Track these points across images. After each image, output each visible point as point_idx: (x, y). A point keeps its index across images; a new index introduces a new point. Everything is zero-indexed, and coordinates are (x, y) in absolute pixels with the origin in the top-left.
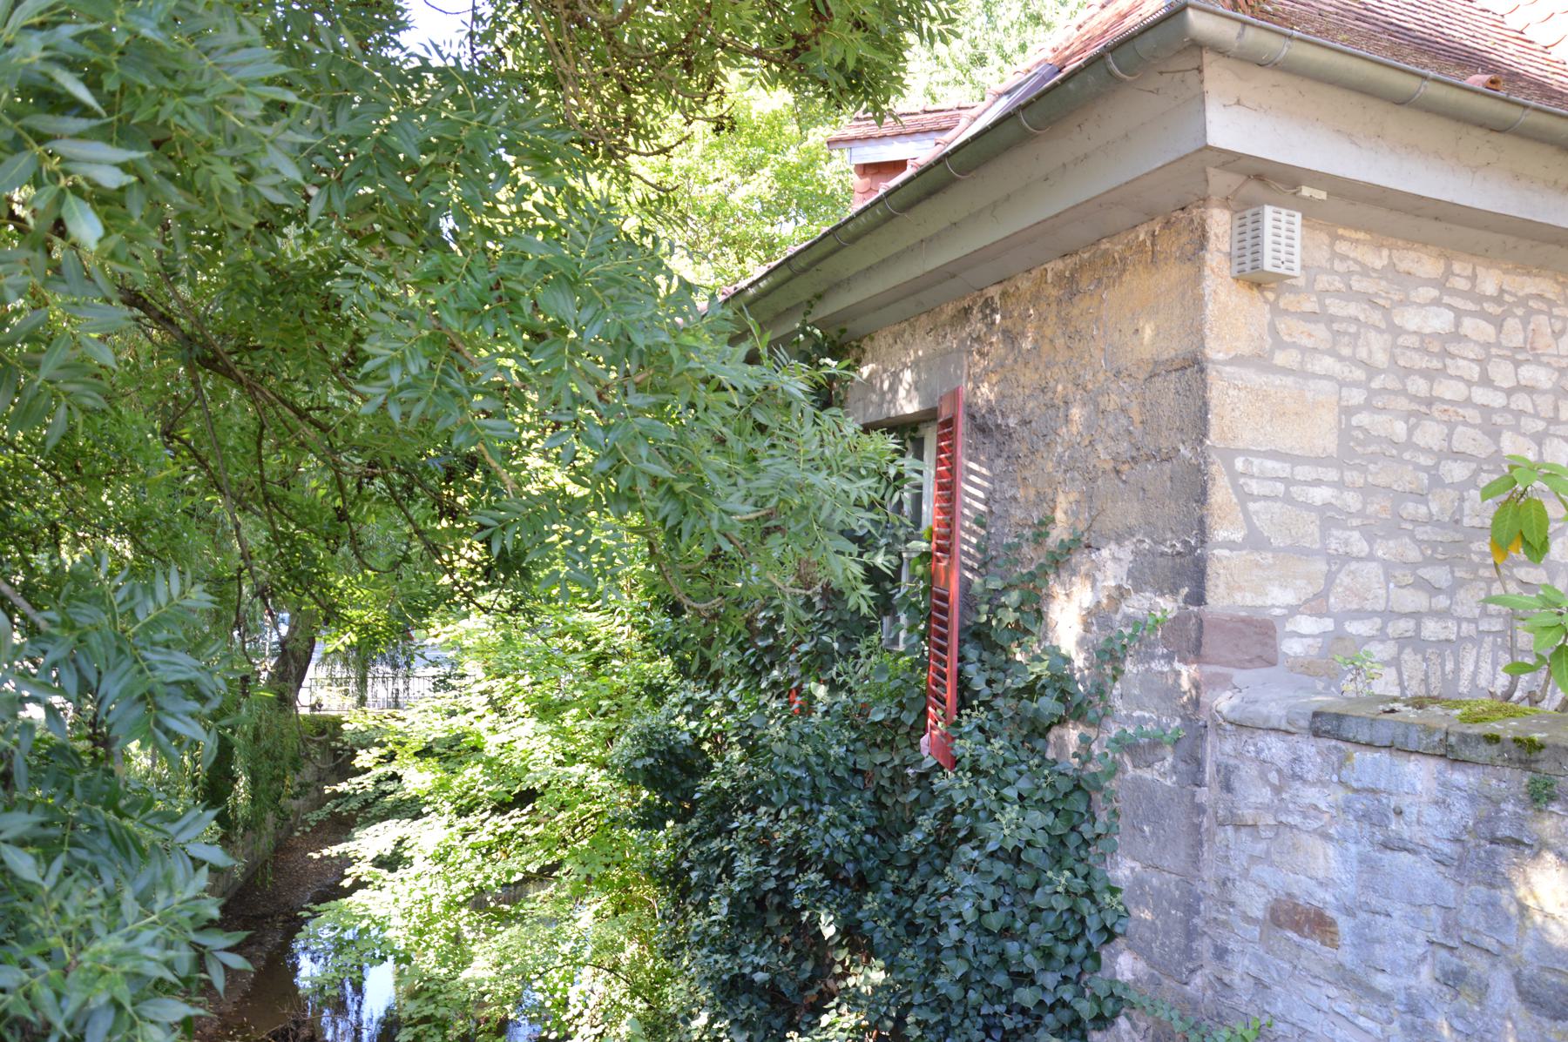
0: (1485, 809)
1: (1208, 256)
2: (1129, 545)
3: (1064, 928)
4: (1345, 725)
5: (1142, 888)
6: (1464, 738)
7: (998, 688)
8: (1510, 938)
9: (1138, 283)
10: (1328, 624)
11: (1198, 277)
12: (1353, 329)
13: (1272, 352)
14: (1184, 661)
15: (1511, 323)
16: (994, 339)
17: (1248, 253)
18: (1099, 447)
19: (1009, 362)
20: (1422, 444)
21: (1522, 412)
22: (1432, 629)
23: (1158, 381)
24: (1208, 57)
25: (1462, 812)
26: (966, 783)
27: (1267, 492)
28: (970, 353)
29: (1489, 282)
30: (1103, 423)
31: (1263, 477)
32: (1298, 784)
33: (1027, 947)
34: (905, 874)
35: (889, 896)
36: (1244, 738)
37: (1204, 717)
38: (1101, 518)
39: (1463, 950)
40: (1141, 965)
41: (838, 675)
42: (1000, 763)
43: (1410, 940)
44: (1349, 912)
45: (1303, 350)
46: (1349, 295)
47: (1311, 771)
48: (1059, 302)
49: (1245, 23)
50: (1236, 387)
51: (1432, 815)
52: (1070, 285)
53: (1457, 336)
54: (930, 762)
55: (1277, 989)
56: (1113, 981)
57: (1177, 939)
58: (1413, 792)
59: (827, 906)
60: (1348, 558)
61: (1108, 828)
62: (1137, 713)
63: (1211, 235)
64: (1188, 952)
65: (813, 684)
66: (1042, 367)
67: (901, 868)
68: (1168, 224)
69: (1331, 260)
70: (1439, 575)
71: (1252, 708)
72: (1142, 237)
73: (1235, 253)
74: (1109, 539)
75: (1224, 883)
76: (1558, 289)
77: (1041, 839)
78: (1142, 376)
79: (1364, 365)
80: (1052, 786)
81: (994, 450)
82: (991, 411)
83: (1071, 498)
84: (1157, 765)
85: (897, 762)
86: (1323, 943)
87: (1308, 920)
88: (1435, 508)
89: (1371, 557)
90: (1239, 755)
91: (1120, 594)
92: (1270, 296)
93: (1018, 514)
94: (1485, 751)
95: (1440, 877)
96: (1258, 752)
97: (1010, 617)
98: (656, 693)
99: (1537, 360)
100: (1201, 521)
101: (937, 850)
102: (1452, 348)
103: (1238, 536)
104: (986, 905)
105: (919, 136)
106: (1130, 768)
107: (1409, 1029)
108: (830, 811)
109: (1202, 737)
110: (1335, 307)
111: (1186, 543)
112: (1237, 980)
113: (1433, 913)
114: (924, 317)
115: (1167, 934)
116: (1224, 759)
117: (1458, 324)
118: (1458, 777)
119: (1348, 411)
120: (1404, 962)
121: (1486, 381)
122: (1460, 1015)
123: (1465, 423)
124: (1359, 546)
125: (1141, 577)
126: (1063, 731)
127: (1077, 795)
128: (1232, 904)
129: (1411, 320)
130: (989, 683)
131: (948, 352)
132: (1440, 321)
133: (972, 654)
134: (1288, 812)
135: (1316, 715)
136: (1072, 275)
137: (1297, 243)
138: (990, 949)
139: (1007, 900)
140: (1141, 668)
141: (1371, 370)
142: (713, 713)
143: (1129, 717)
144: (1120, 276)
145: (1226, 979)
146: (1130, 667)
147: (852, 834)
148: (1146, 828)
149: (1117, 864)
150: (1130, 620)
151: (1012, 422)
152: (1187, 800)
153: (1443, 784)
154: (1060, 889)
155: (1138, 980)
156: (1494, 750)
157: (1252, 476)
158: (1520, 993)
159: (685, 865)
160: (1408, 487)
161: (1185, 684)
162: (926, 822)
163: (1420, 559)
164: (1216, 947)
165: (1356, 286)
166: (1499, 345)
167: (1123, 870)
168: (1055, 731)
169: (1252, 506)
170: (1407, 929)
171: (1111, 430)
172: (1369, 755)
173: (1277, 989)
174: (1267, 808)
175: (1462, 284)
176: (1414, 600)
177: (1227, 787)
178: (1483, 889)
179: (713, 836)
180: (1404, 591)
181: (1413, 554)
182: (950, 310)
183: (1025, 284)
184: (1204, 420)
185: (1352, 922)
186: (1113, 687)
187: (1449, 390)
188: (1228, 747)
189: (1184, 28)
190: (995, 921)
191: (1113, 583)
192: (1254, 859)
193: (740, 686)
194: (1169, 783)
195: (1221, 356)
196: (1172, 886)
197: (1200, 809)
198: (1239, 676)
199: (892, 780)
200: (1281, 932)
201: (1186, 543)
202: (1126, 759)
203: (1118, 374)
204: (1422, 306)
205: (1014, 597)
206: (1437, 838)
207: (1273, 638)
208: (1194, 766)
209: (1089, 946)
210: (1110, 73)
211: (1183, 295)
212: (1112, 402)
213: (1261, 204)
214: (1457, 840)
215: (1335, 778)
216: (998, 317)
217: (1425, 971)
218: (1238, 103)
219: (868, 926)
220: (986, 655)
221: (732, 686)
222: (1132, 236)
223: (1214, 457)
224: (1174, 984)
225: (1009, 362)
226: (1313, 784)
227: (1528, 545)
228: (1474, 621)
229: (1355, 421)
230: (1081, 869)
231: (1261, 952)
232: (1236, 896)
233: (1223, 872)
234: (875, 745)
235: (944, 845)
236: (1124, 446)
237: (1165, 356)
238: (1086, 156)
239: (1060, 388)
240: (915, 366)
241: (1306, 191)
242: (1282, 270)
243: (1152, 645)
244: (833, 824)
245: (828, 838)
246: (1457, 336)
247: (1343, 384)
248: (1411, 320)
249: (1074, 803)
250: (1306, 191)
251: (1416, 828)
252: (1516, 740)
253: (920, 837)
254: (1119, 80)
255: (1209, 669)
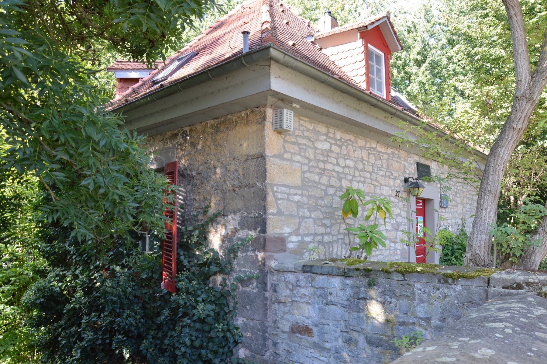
0: (356, 290)
1: (266, 123)
2: (238, 215)
3: (221, 343)
4: (313, 268)
5: (247, 326)
6: (349, 270)
7: (192, 264)
8: (364, 327)
9: (241, 130)
10: (300, 238)
11: (263, 130)
12: (305, 147)
13: (284, 154)
14: (259, 251)
15: (344, 147)
16: (187, 145)
17: (278, 123)
18: (227, 182)
19: (193, 153)
20: (322, 182)
21: (347, 174)
22: (326, 239)
23: (249, 162)
24: (272, 62)
25: (349, 292)
26: (184, 297)
27: (282, 197)
28: (177, 149)
29: (338, 135)
30: (229, 175)
31: (281, 193)
32: (298, 288)
33: (208, 351)
34: (156, 332)
35: (151, 340)
36: (280, 275)
37: (267, 269)
38: (228, 206)
39: (351, 332)
40: (248, 352)
41: (126, 262)
42: (196, 289)
43: (335, 331)
44: (316, 326)
45: (292, 153)
46: (304, 137)
47: (302, 283)
48: (212, 134)
49: (285, 54)
50: (274, 164)
51: (341, 293)
52: (217, 129)
53: (331, 151)
54: (165, 291)
55: (294, 353)
56: (238, 358)
57: (260, 342)
58: (335, 287)
59: (126, 347)
60: (304, 217)
61: (234, 308)
62: (243, 269)
63: (267, 116)
64: (264, 345)
65: (114, 266)
66: (205, 155)
67: (154, 330)
68: (252, 111)
69: (299, 126)
70: (327, 222)
71: (282, 265)
72: (243, 115)
73: (274, 122)
74: (231, 213)
75: (275, 322)
76: (354, 138)
77: (212, 313)
78: (243, 160)
79: (308, 158)
80: (214, 295)
81: (187, 183)
82: (186, 169)
83: (217, 199)
84: (251, 286)
85: (151, 292)
86: (309, 336)
87: (303, 330)
88: (326, 202)
89: (310, 217)
90: (278, 280)
91: (236, 231)
92: (283, 136)
93: (196, 204)
94: (356, 273)
95: (343, 312)
96: (285, 279)
97: (195, 239)
98: (42, 273)
99: (350, 158)
100: (264, 207)
101: (170, 322)
102: (330, 154)
103: (275, 211)
104: (193, 338)
105: (141, 70)
106: (241, 287)
107: (336, 358)
108: (128, 312)
109: (266, 276)
110: (300, 140)
111: (259, 214)
112: (281, 352)
113: (342, 323)
114: (158, 136)
115: (257, 340)
116: (274, 282)
117: (331, 147)
118: (348, 281)
119: (304, 173)
120: (333, 338)
121: (338, 164)
122: (351, 351)
123: (333, 177)
124: (307, 214)
125: (244, 224)
126: (216, 277)
127: (222, 298)
128: (278, 328)
129: (319, 145)
130: (189, 262)
131: (169, 148)
132: (326, 146)
133: (182, 253)
134: (295, 297)
135: (304, 266)
136: (217, 125)
137: (292, 121)
138: (195, 353)
139: (200, 336)
140: (244, 254)
141: (310, 160)
142: (68, 280)
143: (240, 271)
144: (235, 127)
145: (277, 352)
146: (240, 254)
147: (136, 319)
148: (247, 307)
149: (237, 319)
150: (239, 239)
151: (194, 173)
152: (262, 296)
153: (343, 284)
154: (220, 330)
155: (247, 357)
156: (358, 272)
157: (278, 192)
158: (367, 342)
159: (60, 339)
160: (320, 196)
161: (260, 259)
162: (166, 312)
163: (322, 217)
164: (273, 342)
165: (305, 134)
166: (341, 154)
167: (240, 321)
168: (212, 277)
169: (279, 202)
170: (335, 328)
171: (232, 177)
172: (321, 277)
173: (294, 353)
174: (289, 296)
175: (331, 135)
176: (321, 230)
177: (275, 291)
178: (355, 313)
179: (72, 326)
180: (319, 227)
181: (321, 216)
182: (169, 134)
183: (199, 127)
184: (265, 175)
185: (317, 329)
186: (234, 261)
187: (329, 167)
188: (275, 278)
189: (269, 53)
190: (197, 343)
191: (232, 227)
192: (285, 313)
193: (81, 268)
194: (255, 291)
195: (270, 155)
196: (258, 325)
197: (266, 299)
198: (276, 255)
199: (149, 299)
200: (295, 335)
201: (259, 214)
202: (239, 285)
203: (234, 159)
204: (322, 141)
205: (197, 232)
206: (342, 300)
207: (285, 243)
208: (264, 285)
209: (229, 347)
210: (242, 63)
211: (258, 135)
212: (232, 168)
213: (283, 108)
214: (348, 300)
215: (310, 285)
216: (188, 138)
217: (340, 340)
218: (279, 77)
219: (144, 352)
220: (186, 253)
221: (76, 269)
222: (240, 114)
223: (268, 186)
224: (260, 356)
225: (193, 153)
226: (303, 288)
227: (353, 213)
228: (336, 236)
229: (305, 175)
230: (225, 323)
231: (288, 342)
232: (280, 325)
233: (275, 318)
234: (142, 286)
235: (173, 321)
236: (236, 182)
237: (251, 154)
238: (227, 88)
239: (212, 162)
240: (154, 152)
241: (294, 105)
242: (288, 129)
243: (248, 247)
244: (129, 316)
245: (127, 322)
246: (331, 151)
247: (302, 164)
248: (319, 145)
249: (221, 301)
250: (294, 105)
251: (336, 298)
252: (364, 269)
253: (164, 317)
254: (245, 66)
255: (268, 254)
